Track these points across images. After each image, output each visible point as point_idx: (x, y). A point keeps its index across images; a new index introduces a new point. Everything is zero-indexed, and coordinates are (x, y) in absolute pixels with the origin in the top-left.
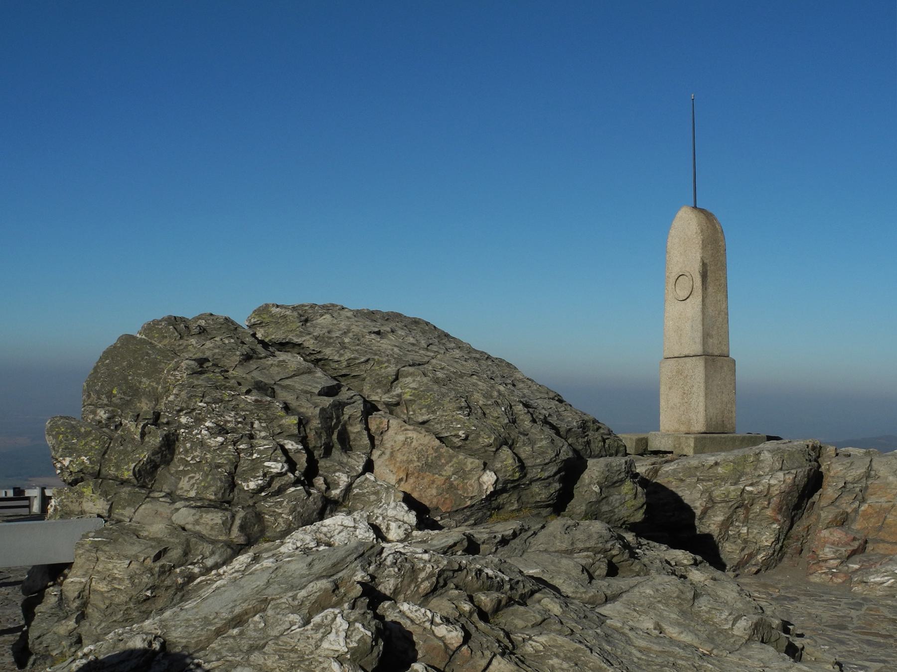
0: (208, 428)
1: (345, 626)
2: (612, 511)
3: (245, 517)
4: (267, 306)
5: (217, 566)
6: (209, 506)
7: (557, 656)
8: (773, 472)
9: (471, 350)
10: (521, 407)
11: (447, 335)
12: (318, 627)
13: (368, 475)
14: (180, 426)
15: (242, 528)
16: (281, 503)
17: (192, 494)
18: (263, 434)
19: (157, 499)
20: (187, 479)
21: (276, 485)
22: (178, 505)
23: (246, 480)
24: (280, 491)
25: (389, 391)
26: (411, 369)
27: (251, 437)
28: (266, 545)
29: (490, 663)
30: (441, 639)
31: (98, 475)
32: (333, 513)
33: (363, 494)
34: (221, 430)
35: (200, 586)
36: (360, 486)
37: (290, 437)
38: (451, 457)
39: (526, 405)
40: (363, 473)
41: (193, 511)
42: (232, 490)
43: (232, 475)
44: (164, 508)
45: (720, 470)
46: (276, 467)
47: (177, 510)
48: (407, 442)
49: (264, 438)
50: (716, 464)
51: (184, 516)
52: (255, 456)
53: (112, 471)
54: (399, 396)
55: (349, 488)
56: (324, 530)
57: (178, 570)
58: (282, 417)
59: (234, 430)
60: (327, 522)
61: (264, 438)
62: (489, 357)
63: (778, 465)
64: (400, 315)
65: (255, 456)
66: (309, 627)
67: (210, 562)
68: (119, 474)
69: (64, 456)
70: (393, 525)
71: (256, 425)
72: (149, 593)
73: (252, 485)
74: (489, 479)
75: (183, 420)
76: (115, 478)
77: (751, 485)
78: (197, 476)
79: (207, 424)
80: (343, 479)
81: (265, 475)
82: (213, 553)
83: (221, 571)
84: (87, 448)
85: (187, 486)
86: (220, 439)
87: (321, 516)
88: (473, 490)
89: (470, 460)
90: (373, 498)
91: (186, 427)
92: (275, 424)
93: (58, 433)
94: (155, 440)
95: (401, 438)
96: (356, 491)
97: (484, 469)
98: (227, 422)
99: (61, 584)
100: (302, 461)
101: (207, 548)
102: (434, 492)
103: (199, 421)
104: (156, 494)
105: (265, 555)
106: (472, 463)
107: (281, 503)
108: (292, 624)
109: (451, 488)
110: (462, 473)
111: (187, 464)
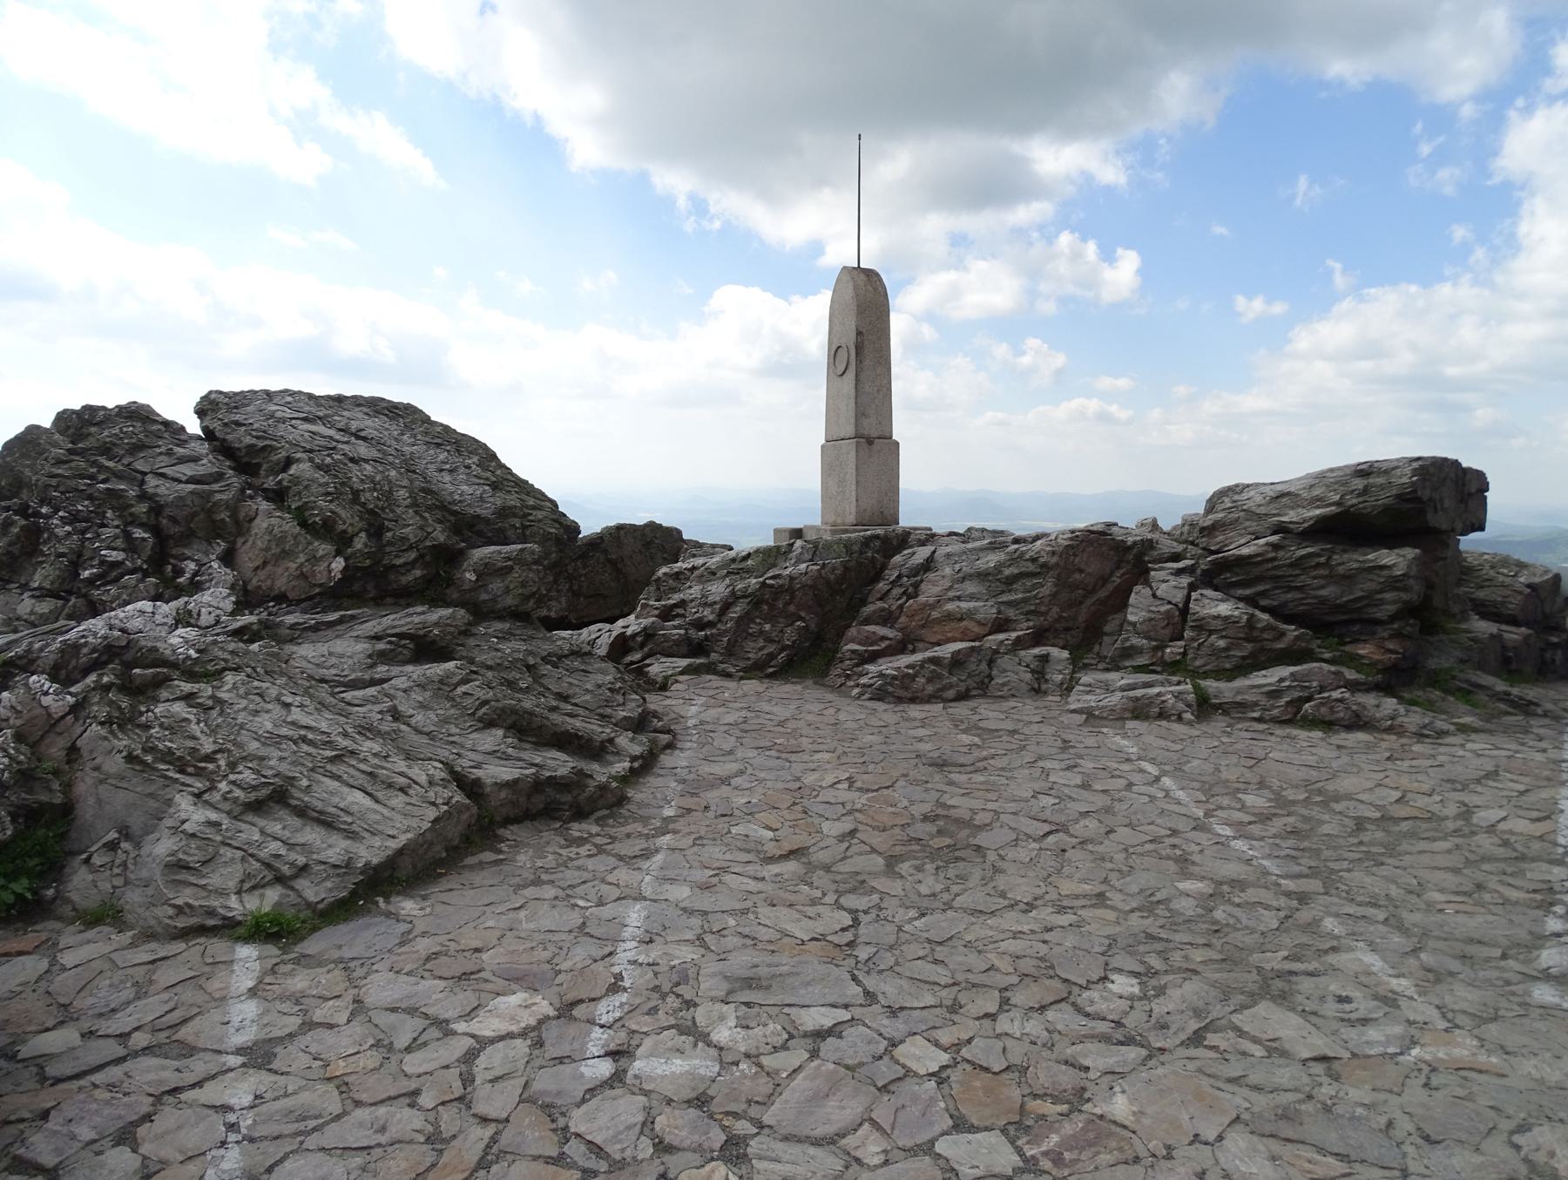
24: (117, 580)
30: (46, 708)
34: (74, 518)
37: (142, 525)
38: (309, 543)
63: (807, 556)
71: (109, 514)
74: (338, 564)
86: (67, 528)
106: (323, 548)
109: (303, 576)
110: (314, 559)
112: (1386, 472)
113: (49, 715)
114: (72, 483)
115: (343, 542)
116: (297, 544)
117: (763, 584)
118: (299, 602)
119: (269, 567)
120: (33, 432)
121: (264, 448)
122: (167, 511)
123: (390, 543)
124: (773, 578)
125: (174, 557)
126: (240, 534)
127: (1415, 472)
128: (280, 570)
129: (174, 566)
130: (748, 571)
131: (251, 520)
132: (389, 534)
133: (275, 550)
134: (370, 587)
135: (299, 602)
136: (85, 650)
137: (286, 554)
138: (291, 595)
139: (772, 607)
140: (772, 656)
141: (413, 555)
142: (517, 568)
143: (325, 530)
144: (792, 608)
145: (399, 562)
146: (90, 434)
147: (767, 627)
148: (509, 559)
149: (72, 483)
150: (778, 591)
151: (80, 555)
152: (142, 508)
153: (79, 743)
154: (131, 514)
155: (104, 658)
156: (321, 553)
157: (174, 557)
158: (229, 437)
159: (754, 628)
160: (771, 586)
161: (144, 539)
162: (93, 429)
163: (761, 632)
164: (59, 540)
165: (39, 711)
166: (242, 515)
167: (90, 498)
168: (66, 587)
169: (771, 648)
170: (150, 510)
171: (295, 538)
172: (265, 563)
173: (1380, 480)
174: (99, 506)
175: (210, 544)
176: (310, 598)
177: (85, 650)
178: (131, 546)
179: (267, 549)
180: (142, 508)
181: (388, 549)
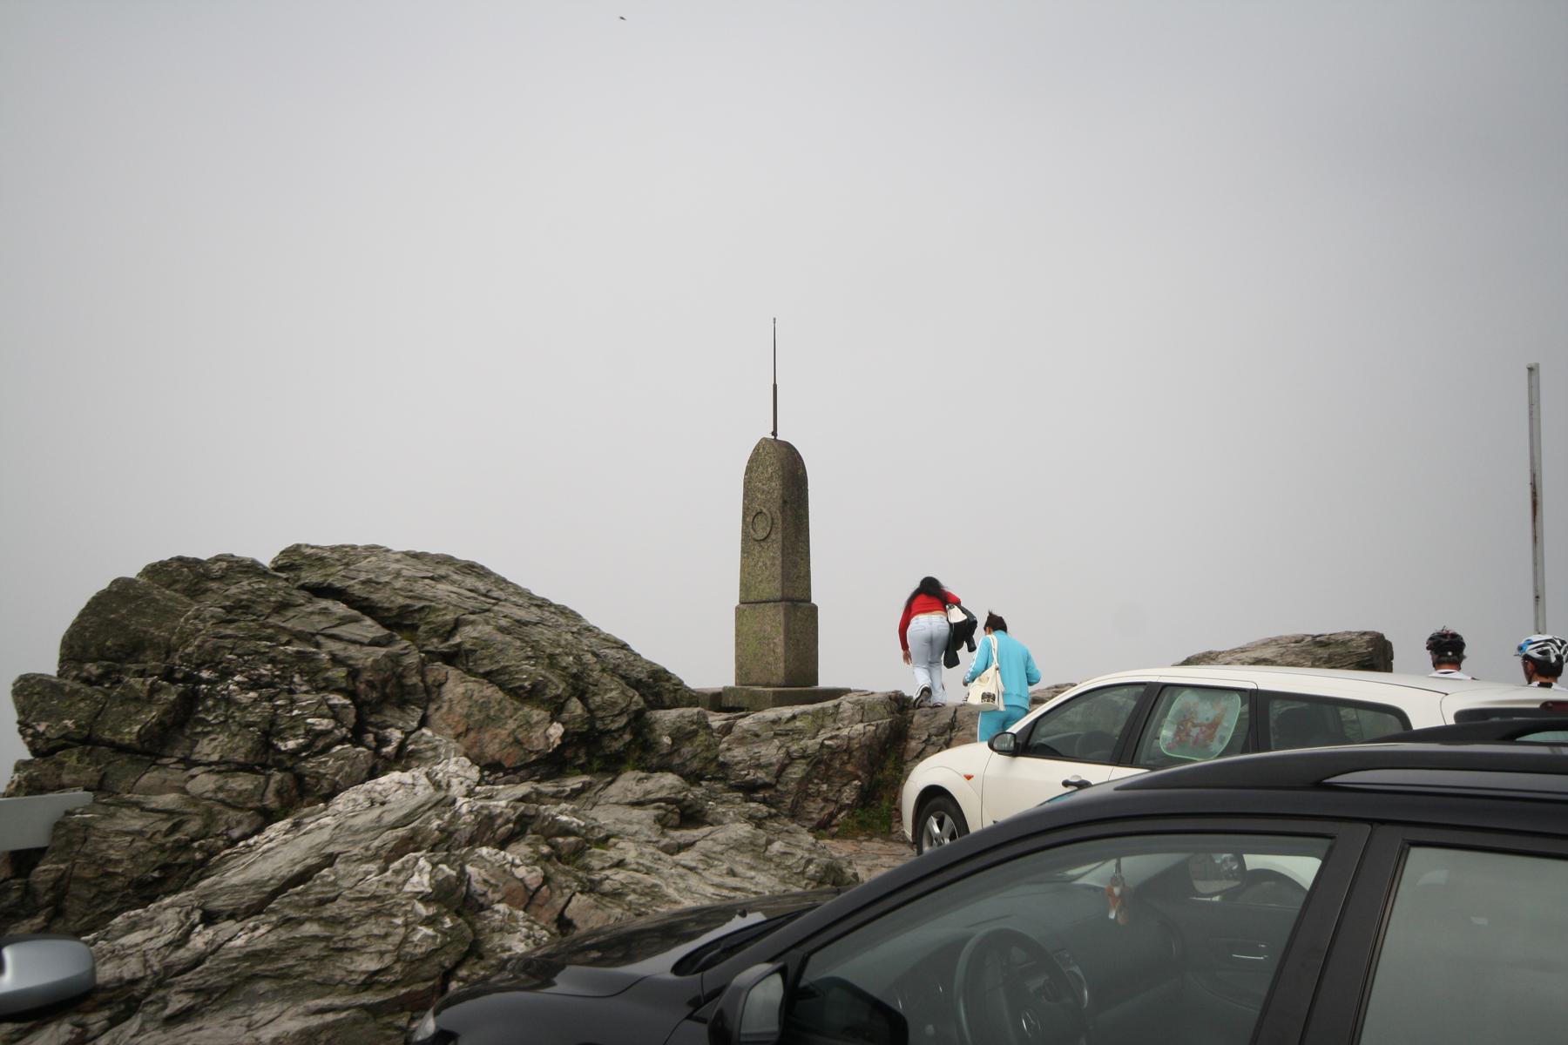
0: (238, 683)
1: (429, 867)
2: (683, 764)
3: (282, 780)
4: (299, 546)
5: (246, 837)
6: (237, 770)
7: (634, 891)
8: (852, 722)
9: (531, 597)
10: (589, 656)
11: (504, 580)
12: (397, 872)
13: (424, 730)
14: (201, 681)
15: (279, 793)
16: (325, 763)
17: (215, 757)
18: (304, 688)
19: (166, 766)
20: (206, 741)
21: (320, 744)
22: (194, 771)
23: (285, 739)
24: (326, 749)
25: (447, 640)
26: (472, 617)
27: (291, 692)
28: (306, 810)
29: (569, 901)
30: (522, 880)
31: (86, 741)
32: (384, 772)
33: (419, 751)
34: (255, 684)
35: (223, 861)
36: (415, 742)
37: (339, 691)
38: (517, 710)
39: (595, 654)
40: (419, 728)
41: (215, 777)
42: (266, 752)
43: (267, 734)
44: (175, 775)
45: (798, 724)
46: (324, 724)
47: (193, 777)
48: (468, 696)
49: (306, 692)
50: (794, 717)
51: (204, 783)
52: (296, 712)
53: (107, 735)
54: (459, 645)
55: (402, 745)
56: (379, 788)
57: (196, 844)
58: (327, 670)
59: (270, 685)
60: (382, 780)
61: (306, 692)
62: (551, 605)
63: (858, 717)
64: (451, 558)
65: (296, 712)
66: (389, 873)
67: (236, 833)
68: (117, 738)
69: (39, 720)
70: (455, 781)
71: (297, 679)
72: (156, 874)
73: (291, 744)
74: (556, 730)
75: (205, 674)
76: (111, 744)
77: (831, 738)
78: (221, 737)
79: (238, 678)
80: (396, 735)
81: (308, 732)
82: (239, 823)
83: (251, 841)
84: (73, 709)
85: (208, 749)
86: (252, 694)
87: (373, 774)
88: (539, 744)
89: (535, 712)
90: (430, 754)
91: (207, 682)
92: (319, 677)
93: (32, 694)
94: (172, 693)
95: (460, 689)
96: (411, 747)
97: (551, 722)
98: (261, 675)
99: (27, 875)
100: (351, 717)
101: (233, 815)
102: (496, 747)
103: (226, 674)
104: (165, 761)
105: (307, 820)
106: (538, 714)
107: (325, 763)
108: (368, 873)
109: (517, 742)
110: (528, 725)
111: (208, 723)
112: (1344, 643)
113: (526, 887)
114: (251, 645)
115: (556, 709)
116: (502, 710)
117: (822, 744)
118: (516, 770)
119: (472, 735)
120: (737, 608)
121: (423, 608)
122: (366, 676)
123: (599, 708)
124: (831, 738)
125: (372, 724)
126: (430, 700)
127: (1370, 643)
128: (487, 736)
129: (376, 735)
130: (801, 732)
131: (441, 685)
132: (598, 699)
133: (478, 716)
134: (582, 753)
135: (516, 770)
136: (500, 821)
137: (490, 721)
138: (506, 765)
139: (829, 767)
140: (832, 816)
141: (623, 720)
142: (701, 732)
143: (533, 695)
144: (849, 768)
145: (614, 726)
146: (207, 590)
147: (825, 787)
148: (693, 723)
149: (251, 645)
150: (834, 752)
151: (272, 723)
152: (339, 673)
153: (568, 914)
154: (326, 679)
155: (518, 829)
156: (535, 718)
157: (372, 724)
158: (373, 596)
159: (812, 789)
160: (829, 747)
161: (344, 706)
162: (214, 585)
163: (819, 792)
164: (244, 708)
165: (514, 884)
166: (430, 680)
167: (273, 661)
168: (259, 759)
169: (832, 808)
170: (349, 674)
171: (500, 703)
172: (468, 730)
173: (1339, 650)
174: (282, 670)
175: (403, 710)
176: (527, 766)
177: (500, 821)
178: (335, 713)
179: (468, 716)
180: (339, 673)
181: (600, 714)
